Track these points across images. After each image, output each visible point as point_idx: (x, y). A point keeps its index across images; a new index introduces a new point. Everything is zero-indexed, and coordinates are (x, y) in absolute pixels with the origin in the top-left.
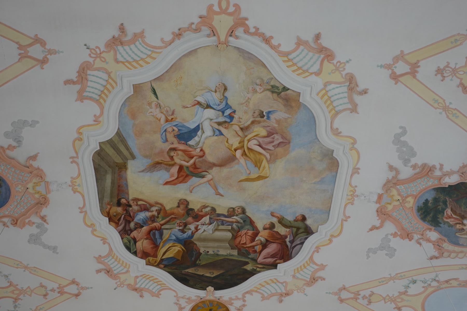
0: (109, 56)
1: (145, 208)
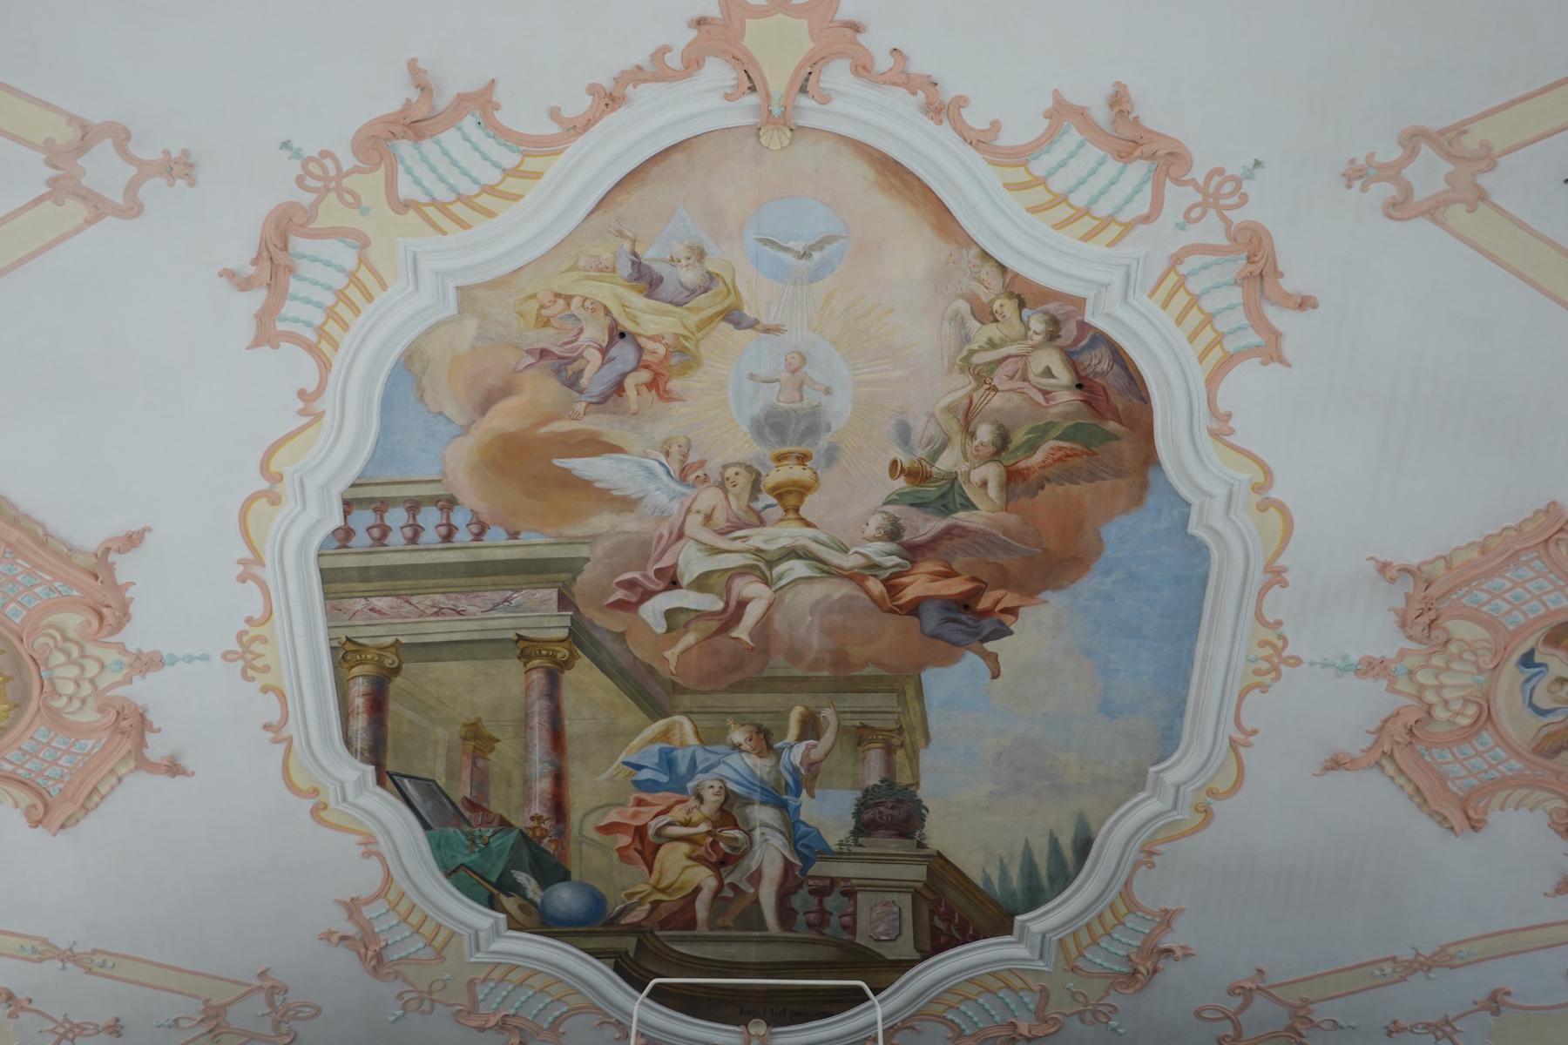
0: (370, 185)
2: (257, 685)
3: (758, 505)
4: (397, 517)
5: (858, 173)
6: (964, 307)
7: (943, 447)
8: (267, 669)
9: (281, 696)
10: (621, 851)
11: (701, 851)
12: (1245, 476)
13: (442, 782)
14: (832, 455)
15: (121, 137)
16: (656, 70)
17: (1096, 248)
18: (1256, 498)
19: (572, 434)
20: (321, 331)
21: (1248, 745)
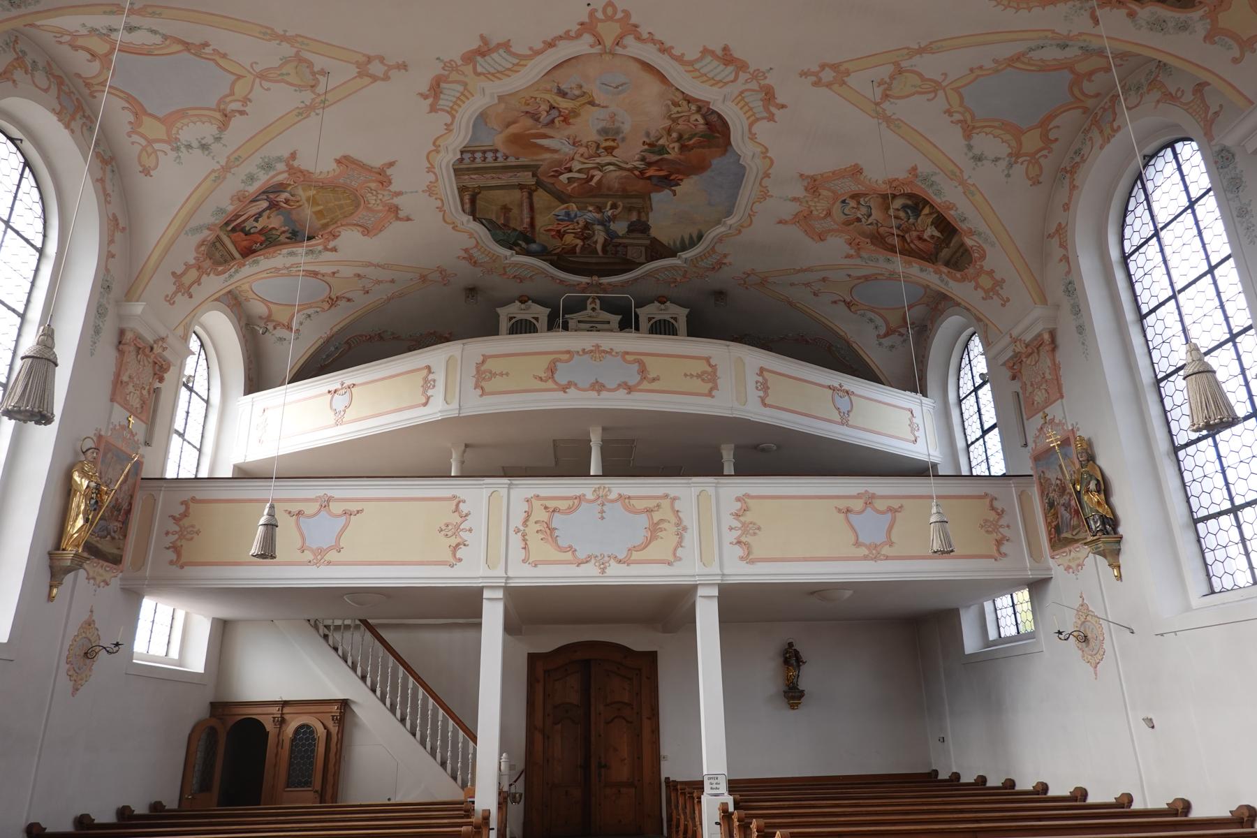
0: (468, 69)
1: (95, 322)
2: (434, 198)
3: (598, 152)
4: (479, 155)
5: (635, 67)
6: (670, 103)
7: (660, 139)
8: (437, 194)
9: (442, 200)
10: (552, 236)
11: (577, 236)
12: (759, 150)
13: (494, 219)
14: (623, 139)
15: (382, 59)
16: (567, 36)
17: (715, 89)
18: (763, 156)
19: (537, 133)
20: (452, 108)
21: (754, 216)
